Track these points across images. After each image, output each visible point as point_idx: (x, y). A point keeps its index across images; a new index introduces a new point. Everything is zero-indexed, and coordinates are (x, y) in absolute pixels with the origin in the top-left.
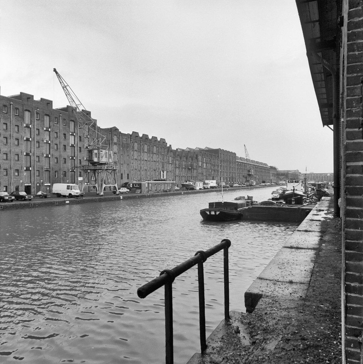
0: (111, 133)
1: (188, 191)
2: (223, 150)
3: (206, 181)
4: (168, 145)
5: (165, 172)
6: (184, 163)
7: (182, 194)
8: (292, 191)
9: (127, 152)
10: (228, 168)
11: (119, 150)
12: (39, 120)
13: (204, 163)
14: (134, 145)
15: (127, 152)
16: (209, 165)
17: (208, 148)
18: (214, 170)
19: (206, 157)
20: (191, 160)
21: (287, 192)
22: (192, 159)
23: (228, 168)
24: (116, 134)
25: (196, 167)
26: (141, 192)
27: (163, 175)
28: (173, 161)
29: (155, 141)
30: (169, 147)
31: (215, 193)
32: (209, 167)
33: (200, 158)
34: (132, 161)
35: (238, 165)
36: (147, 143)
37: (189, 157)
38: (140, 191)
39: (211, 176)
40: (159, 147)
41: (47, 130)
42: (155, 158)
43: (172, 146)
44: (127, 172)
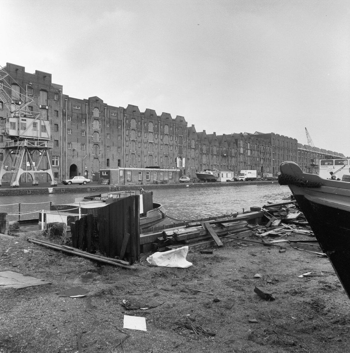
0: (89, 105)
1: (205, 183)
3: (242, 172)
4: (189, 125)
5: (184, 159)
6: (215, 149)
7: (273, 184)
9: (118, 131)
11: (103, 128)
12: (33, 96)
13: (248, 149)
14: (129, 122)
15: (118, 131)
16: (256, 153)
17: (258, 132)
18: (264, 159)
19: (251, 143)
22: (229, 145)
24: (98, 106)
25: (236, 154)
26: (109, 183)
27: (181, 163)
28: (197, 146)
29: (167, 118)
30: (190, 127)
31: (255, 186)
32: (256, 155)
33: (241, 143)
35: (300, 154)
36: (153, 121)
37: (223, 141)
38: (107, 181)
40: (173, 127)
41: (43, 108)
42: (166, 140)
44: (117, 158)
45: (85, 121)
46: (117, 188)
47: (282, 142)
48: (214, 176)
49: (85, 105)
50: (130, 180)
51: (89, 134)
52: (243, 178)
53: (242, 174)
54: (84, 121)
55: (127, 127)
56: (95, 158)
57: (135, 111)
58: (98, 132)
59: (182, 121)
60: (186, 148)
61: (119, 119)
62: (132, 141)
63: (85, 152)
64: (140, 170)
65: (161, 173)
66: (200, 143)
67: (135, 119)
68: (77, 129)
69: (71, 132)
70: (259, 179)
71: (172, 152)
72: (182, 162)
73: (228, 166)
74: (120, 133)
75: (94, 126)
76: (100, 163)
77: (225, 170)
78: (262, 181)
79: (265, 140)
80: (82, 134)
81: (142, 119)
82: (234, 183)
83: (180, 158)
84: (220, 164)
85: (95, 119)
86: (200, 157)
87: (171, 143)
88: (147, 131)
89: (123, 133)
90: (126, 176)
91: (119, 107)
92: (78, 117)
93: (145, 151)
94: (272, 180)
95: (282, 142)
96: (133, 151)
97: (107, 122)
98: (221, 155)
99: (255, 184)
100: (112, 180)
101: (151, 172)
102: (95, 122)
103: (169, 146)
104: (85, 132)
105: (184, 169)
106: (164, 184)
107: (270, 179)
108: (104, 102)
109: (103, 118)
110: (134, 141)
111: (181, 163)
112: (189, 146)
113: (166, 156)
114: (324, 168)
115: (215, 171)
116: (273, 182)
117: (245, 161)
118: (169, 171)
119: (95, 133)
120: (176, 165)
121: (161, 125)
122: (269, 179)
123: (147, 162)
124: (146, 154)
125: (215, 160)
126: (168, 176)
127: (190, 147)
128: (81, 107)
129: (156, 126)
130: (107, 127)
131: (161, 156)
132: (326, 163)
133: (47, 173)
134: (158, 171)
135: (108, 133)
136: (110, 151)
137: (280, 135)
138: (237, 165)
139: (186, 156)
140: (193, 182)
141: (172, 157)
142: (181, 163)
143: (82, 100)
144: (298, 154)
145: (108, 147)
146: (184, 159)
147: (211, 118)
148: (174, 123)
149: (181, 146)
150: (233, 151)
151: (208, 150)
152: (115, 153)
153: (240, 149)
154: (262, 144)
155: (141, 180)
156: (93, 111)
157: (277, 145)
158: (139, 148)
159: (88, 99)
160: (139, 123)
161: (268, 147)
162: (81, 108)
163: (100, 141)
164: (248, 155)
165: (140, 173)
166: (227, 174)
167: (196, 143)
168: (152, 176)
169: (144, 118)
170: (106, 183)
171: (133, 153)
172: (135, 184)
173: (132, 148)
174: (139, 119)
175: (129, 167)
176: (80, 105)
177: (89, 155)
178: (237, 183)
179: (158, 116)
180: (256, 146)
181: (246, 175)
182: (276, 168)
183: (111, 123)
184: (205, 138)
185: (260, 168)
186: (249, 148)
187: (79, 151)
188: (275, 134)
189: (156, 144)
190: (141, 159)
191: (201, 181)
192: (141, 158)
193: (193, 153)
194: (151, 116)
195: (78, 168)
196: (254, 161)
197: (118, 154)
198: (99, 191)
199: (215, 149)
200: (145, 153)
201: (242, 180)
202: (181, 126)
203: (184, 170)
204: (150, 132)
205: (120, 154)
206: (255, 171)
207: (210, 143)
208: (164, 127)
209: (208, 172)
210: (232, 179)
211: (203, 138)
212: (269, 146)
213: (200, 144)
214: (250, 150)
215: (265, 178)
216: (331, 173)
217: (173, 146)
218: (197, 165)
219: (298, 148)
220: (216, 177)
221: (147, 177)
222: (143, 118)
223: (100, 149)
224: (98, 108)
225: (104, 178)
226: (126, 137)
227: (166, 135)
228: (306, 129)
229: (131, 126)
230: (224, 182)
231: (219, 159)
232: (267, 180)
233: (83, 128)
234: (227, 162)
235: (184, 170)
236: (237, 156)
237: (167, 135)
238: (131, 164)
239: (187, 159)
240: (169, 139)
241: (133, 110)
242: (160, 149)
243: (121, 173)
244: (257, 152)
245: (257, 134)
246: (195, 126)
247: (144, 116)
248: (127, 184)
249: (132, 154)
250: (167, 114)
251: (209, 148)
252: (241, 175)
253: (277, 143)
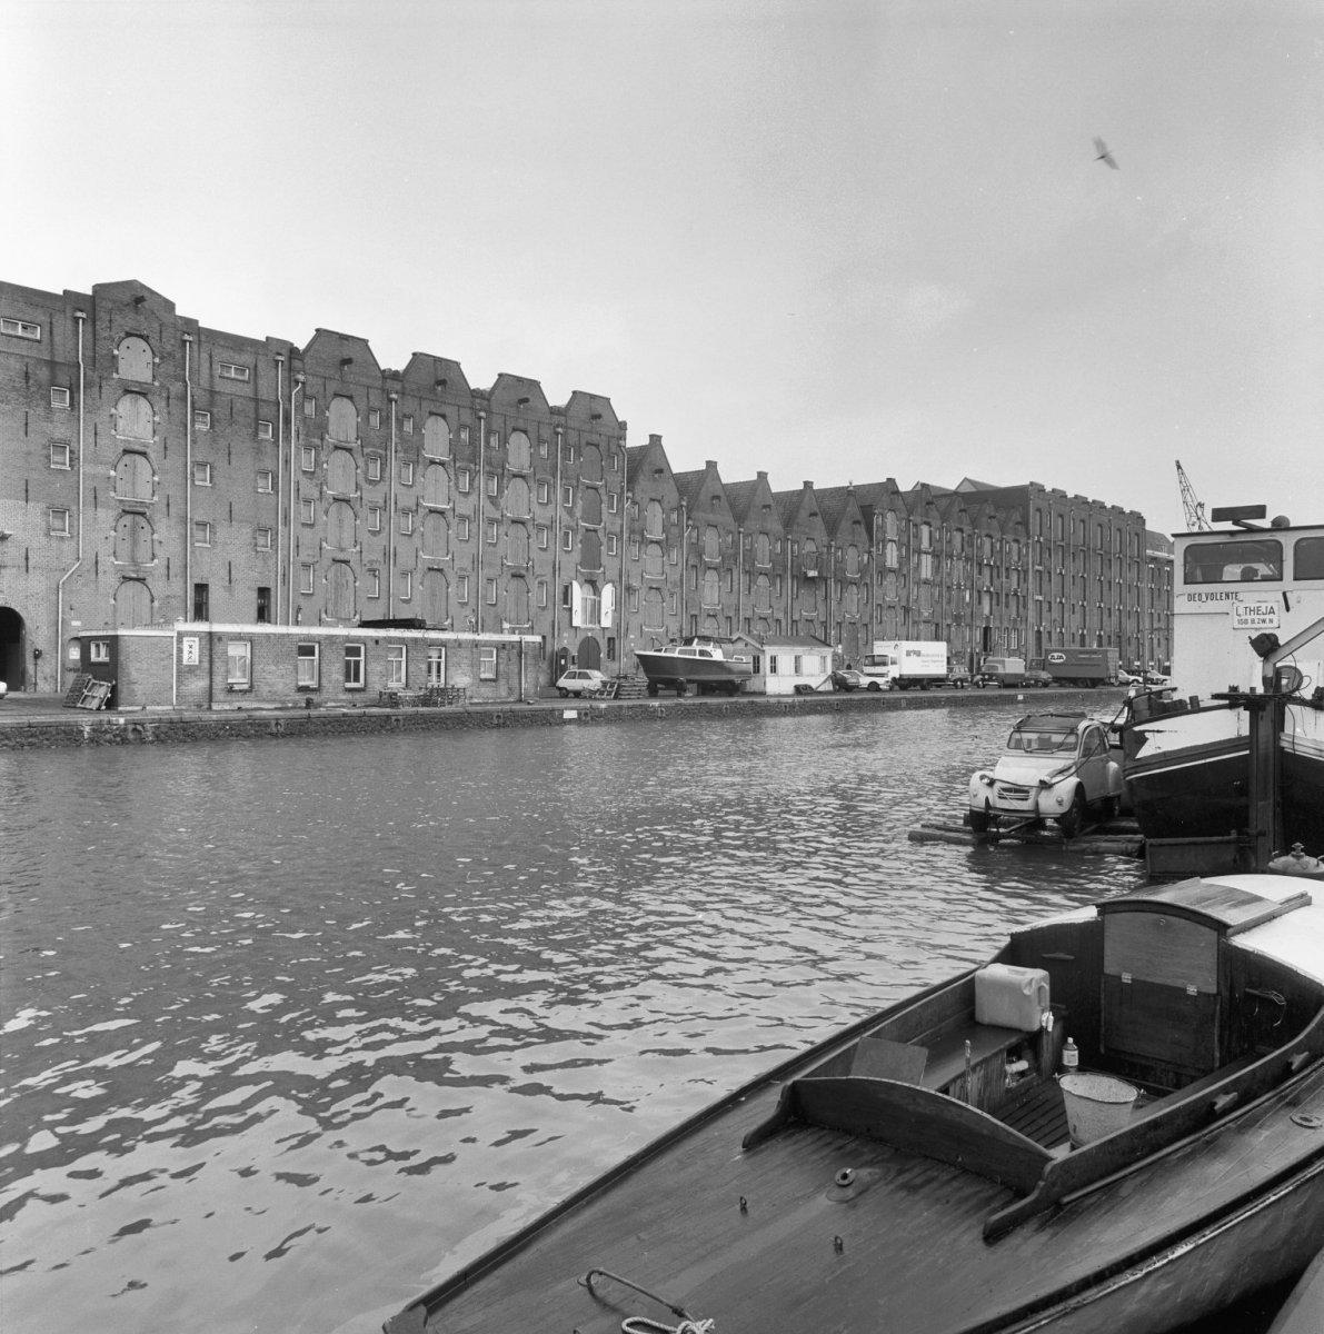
2: (1059, 495)
3: (880, 648)
4: (636, 438)
5: (608, 592)
6: (763, 546)
7: (1019, 702)
8: (1231, 725)
10: (1093, 590)
13: (919, 552)
16: (958, 570)
18: (996, 597)
19: (998, 535)
20: (821, 535)
21: (1168, 737)
22: (832, 530)
23: (1093, 590)
26: (111, 703)
28: (675, 531)
33: (890, 524)
34: (300, 513)
37: (803, 514)
38: (102, 691)
39: (970, 626)
42: (518, 499)
43: (770, 478)
45: (72, 398)
46: (130, 727)
47: (1078, 522)
48: (732, 666)
49: (69, 324)
50: (246, 687)
51: (96, 460)
52: (882, 675)
53: (877, 659)
54: (68, 400)
55: (307, 435)
56: (126, 579)
57: (347, 361)
58: (144, 454)
59: (599, 416)
60: (620, 539)
61: (264, 394)
62: (336, 500)
63: (68, 547)
64: (309, 638)
65: (434, 654)
66: (688, 518)
67: (350, 398)
68: (22, 433)
69: (71, 460)
70: (962, 680)
71: (548, 556)
72: (600, 602)
73: (824, 624)
74: (268, 464)
75: (121, 423)
76: (156, 604)
77: (794, 639)
78: (971, 692)
79: (1001, 515)
80: (55, 458)
81: (390, 400)
82: (828, 701)
83: (588, 587)
84: (786, 613)
85: (127, 392)
86: (689, 580)
87: (543, 515)
88: (414, 453)
89: (287, 462)
90: (218, 664)
91: (267, 338)
92: (27, 376)
93: (404, 550)
94: (1023, 687)
95: (1078, 522)
96: (342, 550)
97: (193, 409)
98: (793, 577)
99: (933, 704)
100: (135, 687)
101: (371, 645)
102: (126, 405)
103: (530, 528)
104: (71, 452)
105: (608, 635)
106: (435, 704)
107: (1010, 683)
108: (179, 312)
109: (176, 388)
110: (347, 501)
111: (595, 612)
112: (632, 532)
113: (514, 576)
114: (1211, 606)
115: (740, 645)
116: (1020, 697)
117: (908, 601)
118: (476, 644)
119: (127, 459)
120: (567, 614)
121: (489, 432)
122: (1007, 682)
123: (417, 598)
124: (411, 563)
125: (764, 598)
126: (475, 665)
127: (639, 536)
128: (47, 329)
129: (464, 435)
130: (193, 432)
131: (492, 573)
132: (1233, 571)
133: (1295, 668)
134: (415, 640)
135: (199, 458)
136: (213, 547)
137: (1070, 495)
138: (871, 618)
139: (621, 577)
140: (615, 698)
141: (548, 578)
142: (595, 612)
143: (56, 296)
144: (1146, 575)
145: (202, 525)
146: (608, 592)
147: (738, 406)
148: (558, 426)
149: (595, 531)
150: (852, 559)
151: (730, 551)
152: (241, 558)
153: (884, 547)
154: (954, 525)
155: (313, 684)
156: (116, 352)
157: (1056, 535)
158: (374, 533)
159: (89, 292)
160: (375, 420)
161: (1015, 546)
162: (46, 335)
163: (156, 498)
164: (923, 576)
165: (308, 651)
166: (797, 659)
167: (668, 517)
168: (376, 667)
169: (403, 393)
170: (94, 704)
171: (341, 556)
172: (273, 706)
173: (338, 532)
174: (371, 398)
175: (320, 622)
176: (43, 318)
177: (89, 564)
178: (846, 701)
179: (474, 390)
180: (958, 536)
181: (893, 663)
182: (1050, 633)
183: (221, 411)
184: (765, 507)
185: (978, 635)
186: (925, 544)
187: (37, 541)
188: (1048, 489)
189: (463, 518)
190: (384, 587)
191: (666, 692)
192: (384, 583)
193: (653, 564)
194: (440, 388)
195: (28, 623)
196: (949, 602)
197: (259, 563)
198: (13, 748)
199: (763, 546)
200: (406, 560)
201: (874, 687)
202: (595, 438)
203: (611, 640)
204: (432, 462)
205: (271, 562)
206: (940, 648)
207: (740, 518)
208: (504, 441)
209: (698, 648)
210: (825, 682)
211: (699, 491)
212: (1017, 541)
213: (690, 522)
214: (929, 557)
215: (991, 675)
216: (1266, 646)
217: (550, 528)
218: (674, 619)
219: (1149, 552)
220: (742, 672)
221: (351, 672)
222: (394, 396)
223: (156, 536)
224: (145, 338)
225: (94, 678)
226: (304, 481)
227: (515, 476)
228: (1179, 467)
229: (330, 428)
230: (780, 696)
231: (784, 595)
232: (1000, 687)
233: (60, 432)
234: (821, 608)
235: (611, 640)
236: (872, 578)
237: (523, 477)
238: (330, 607)
239: (626, 591)
240: (533, 496)
241: (339, 357)
242: (485, 543)
243: (192, 652)
244: (961, 564)
245: (968, 490)
246: (769, 478)
247: (398, 386)
248: (227, 707)
249: (335, 561)
250: (519, 380)
251: (735, 544)
252: (875, 664)
253: (1056, 527)
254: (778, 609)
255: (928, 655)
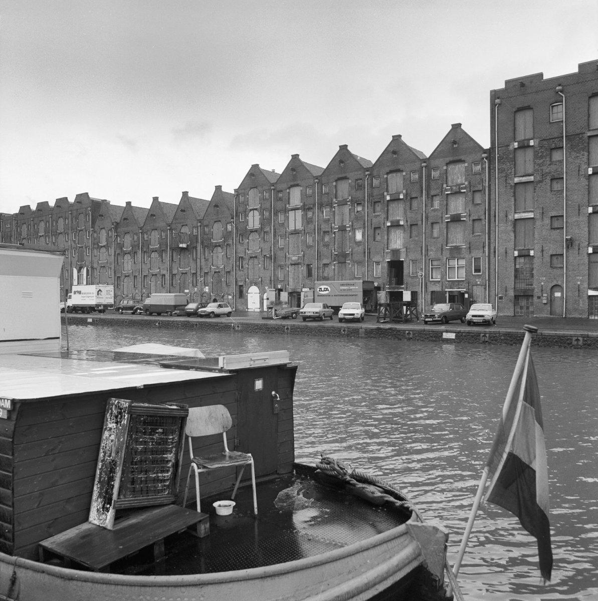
127: (96, 245)
151: (136, 243)
254: (164, 269)
255: (85, 294)
